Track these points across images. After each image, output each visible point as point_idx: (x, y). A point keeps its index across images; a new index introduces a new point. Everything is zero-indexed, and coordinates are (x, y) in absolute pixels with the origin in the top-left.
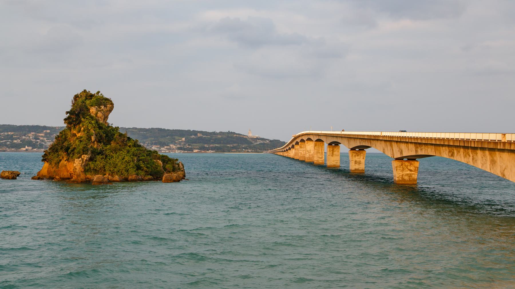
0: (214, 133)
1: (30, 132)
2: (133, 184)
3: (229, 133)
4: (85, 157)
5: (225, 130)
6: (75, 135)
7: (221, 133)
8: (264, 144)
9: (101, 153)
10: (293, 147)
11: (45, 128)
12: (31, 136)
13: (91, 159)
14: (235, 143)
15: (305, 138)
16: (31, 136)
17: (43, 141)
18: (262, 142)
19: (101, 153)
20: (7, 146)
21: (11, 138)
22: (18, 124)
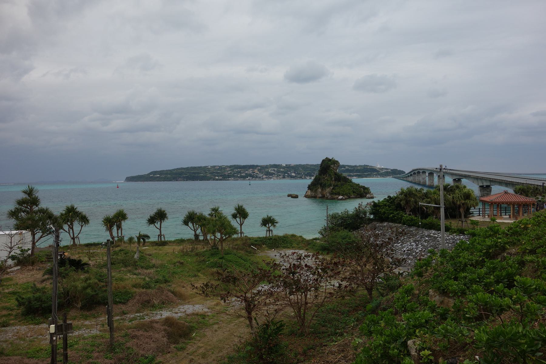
0: (356, 166)
1: (249, 168)
2: (341, 201)
3: (365, 165)
4: (332, 188)
5: (363, 164)
6: (324, 178)
7: (360, 166)
8: (387, 172)
9: (337, 186)
10: (411, 175)
11: (257, 166)
12: (250, 171)
13: (333, 189)
14: (369, 171)
15: (416, 172)
16: (250, 171)
17: (257, 174)
18: (386, 170)
19: (337, 186)
20: (238, 177)
21: (240, 172)
22: (242, 164)
